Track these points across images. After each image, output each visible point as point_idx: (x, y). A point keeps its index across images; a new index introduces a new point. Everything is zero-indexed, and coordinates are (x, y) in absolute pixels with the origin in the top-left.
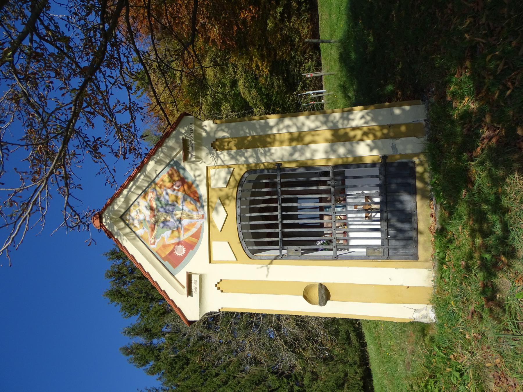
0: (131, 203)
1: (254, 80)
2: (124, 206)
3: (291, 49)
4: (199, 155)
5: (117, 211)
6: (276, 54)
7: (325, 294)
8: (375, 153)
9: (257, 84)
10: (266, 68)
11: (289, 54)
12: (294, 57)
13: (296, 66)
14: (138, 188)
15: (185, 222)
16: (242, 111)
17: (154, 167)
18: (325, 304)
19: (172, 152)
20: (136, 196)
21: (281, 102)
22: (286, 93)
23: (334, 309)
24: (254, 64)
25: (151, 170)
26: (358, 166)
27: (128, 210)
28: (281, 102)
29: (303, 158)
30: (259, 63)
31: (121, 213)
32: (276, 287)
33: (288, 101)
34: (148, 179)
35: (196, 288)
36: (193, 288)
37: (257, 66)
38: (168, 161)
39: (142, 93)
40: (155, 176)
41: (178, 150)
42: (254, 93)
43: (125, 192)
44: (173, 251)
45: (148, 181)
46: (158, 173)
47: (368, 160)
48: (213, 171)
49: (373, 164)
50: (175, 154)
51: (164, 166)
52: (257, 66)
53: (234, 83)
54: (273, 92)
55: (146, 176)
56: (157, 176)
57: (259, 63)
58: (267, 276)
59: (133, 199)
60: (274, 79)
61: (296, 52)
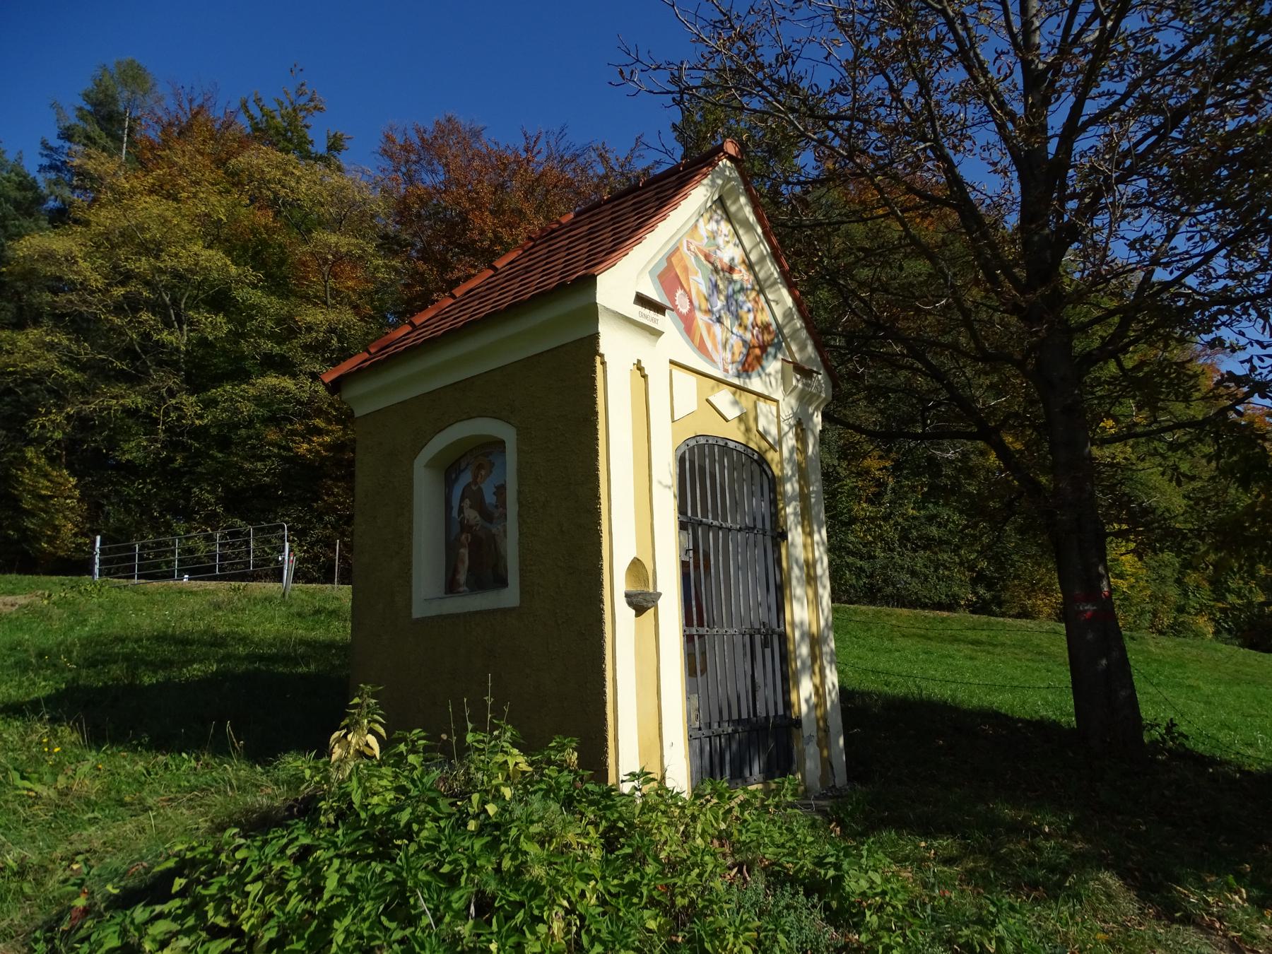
0: (741, 232)
1: (276, 413)
2: (740, 215)
3: (341, 517)
4: (794, 394)
5: (737, 199)
6: (337, 479)
7: (642, 603)
8: (804, 708)
9: (266, 421)
10: (309, 451)
11: (331, 509)
12: (321, 519)
13: (299, 519)
14: (762, 259)
15: (717, 328)
16: (185, 362)
17: (785, 303)
18: (630, 604)
19: (798, 345)
20: (748, 245)
21: (199, 469)
22: (227, 488)
23: (622, 625)
24: (322, 425)
25: (781, 295)
26: (785, 679)
27: (729, 218)
28: (199, 469)
29: (794, 582)
30: (327, 439)
31: (728, 203)
32: (639, 524)
33: (201, 490)
34: (769, 283)
35: (646, 317)
36: (647, 311)
37: (319, 432)
38: (786, 331)
39: (251, 118)
40: (770, 297)
41: (797, 356)
42: (247, 408)
43: (759, 230)
44: (682, 287)
45: (766, 280)
46: (773, 304)
47: (794, 697)
48: (777, 413)
49: (788, 705)
50: (794, 348)
51: (780, 320)
52: (319, 432)
53: (283, 365)
54: (237, 455)
55: (775, 283)
56: (767, 301)
57: (327, 439)
58: (660, 483)
59: (745, 239)
60: (274, 464)
61: (333, 527)
